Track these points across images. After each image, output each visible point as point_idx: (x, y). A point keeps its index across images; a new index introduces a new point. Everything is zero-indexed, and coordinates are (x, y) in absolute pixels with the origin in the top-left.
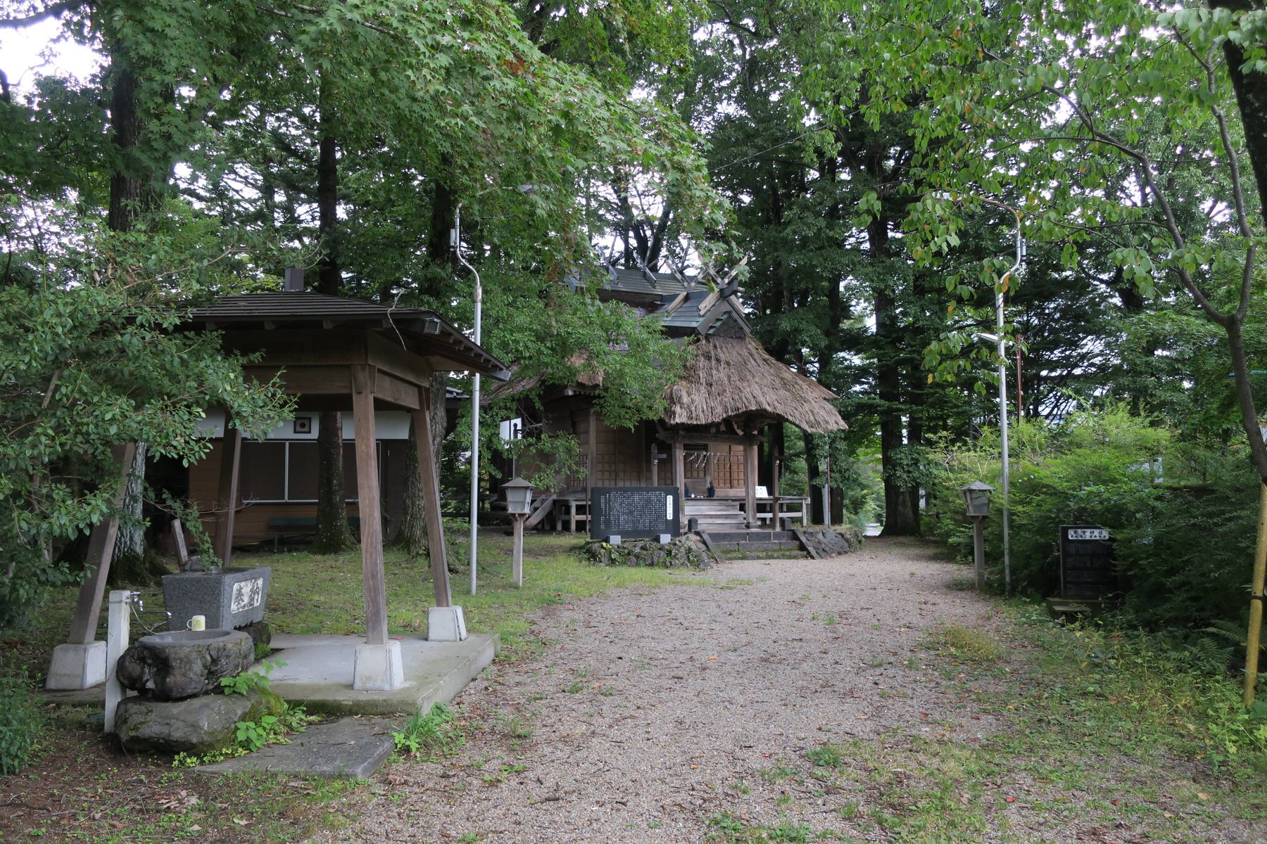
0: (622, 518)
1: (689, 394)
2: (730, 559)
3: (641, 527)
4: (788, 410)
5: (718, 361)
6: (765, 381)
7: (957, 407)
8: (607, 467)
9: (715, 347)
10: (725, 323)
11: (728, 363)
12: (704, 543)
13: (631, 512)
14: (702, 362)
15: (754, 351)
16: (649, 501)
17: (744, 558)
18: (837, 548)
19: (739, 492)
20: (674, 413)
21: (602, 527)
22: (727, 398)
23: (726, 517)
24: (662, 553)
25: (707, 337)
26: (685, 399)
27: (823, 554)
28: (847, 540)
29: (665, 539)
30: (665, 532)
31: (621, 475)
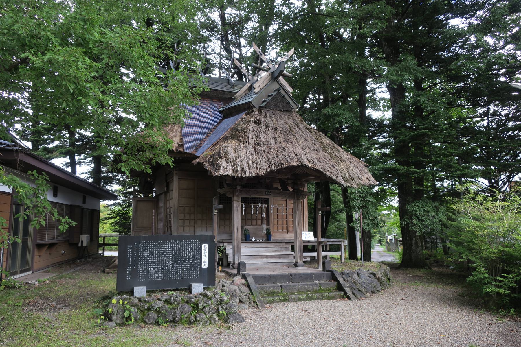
0: (151, 268)
1: (236, 151)
2: (272, 302)
3: (172, 276)
4: (326, 167)
5: (267, 126)
6: (307, 144)
7: (460, 170)
8: (187, 217)
9: (266, 116)
10: (274, 98)
11: (276, 129)
12: (248, 286)
13: (162, 261)
14: (253, 127)
15: (299, 122)
16: (182, 249)
17: (285, 300)
18: (370, 288)
19: (289, 236)
20: (219, 166)
21: (128, 278)
22: (272, 156)
23: (280, 256)
24: (187, 307)
25: (260, 109)
26: (232, 154)
27: (358, 294)
28: (379, 279)
29: (198, 288)
30: (197, 281)
31: (199, 223)
